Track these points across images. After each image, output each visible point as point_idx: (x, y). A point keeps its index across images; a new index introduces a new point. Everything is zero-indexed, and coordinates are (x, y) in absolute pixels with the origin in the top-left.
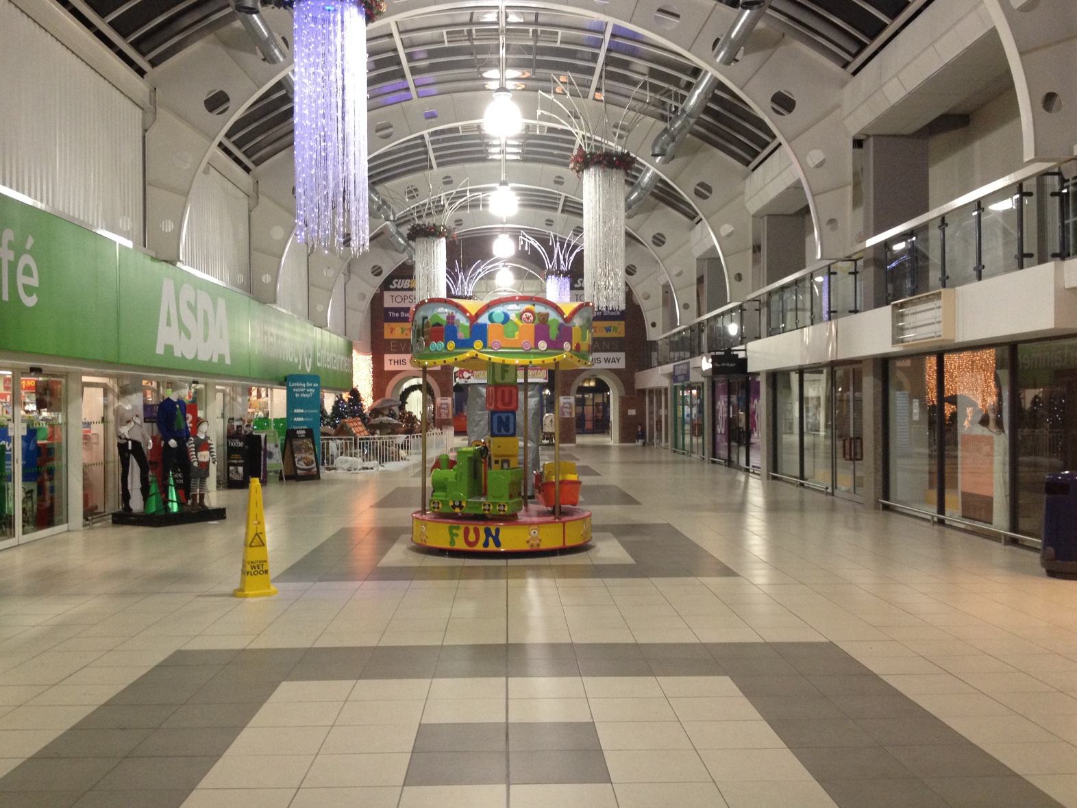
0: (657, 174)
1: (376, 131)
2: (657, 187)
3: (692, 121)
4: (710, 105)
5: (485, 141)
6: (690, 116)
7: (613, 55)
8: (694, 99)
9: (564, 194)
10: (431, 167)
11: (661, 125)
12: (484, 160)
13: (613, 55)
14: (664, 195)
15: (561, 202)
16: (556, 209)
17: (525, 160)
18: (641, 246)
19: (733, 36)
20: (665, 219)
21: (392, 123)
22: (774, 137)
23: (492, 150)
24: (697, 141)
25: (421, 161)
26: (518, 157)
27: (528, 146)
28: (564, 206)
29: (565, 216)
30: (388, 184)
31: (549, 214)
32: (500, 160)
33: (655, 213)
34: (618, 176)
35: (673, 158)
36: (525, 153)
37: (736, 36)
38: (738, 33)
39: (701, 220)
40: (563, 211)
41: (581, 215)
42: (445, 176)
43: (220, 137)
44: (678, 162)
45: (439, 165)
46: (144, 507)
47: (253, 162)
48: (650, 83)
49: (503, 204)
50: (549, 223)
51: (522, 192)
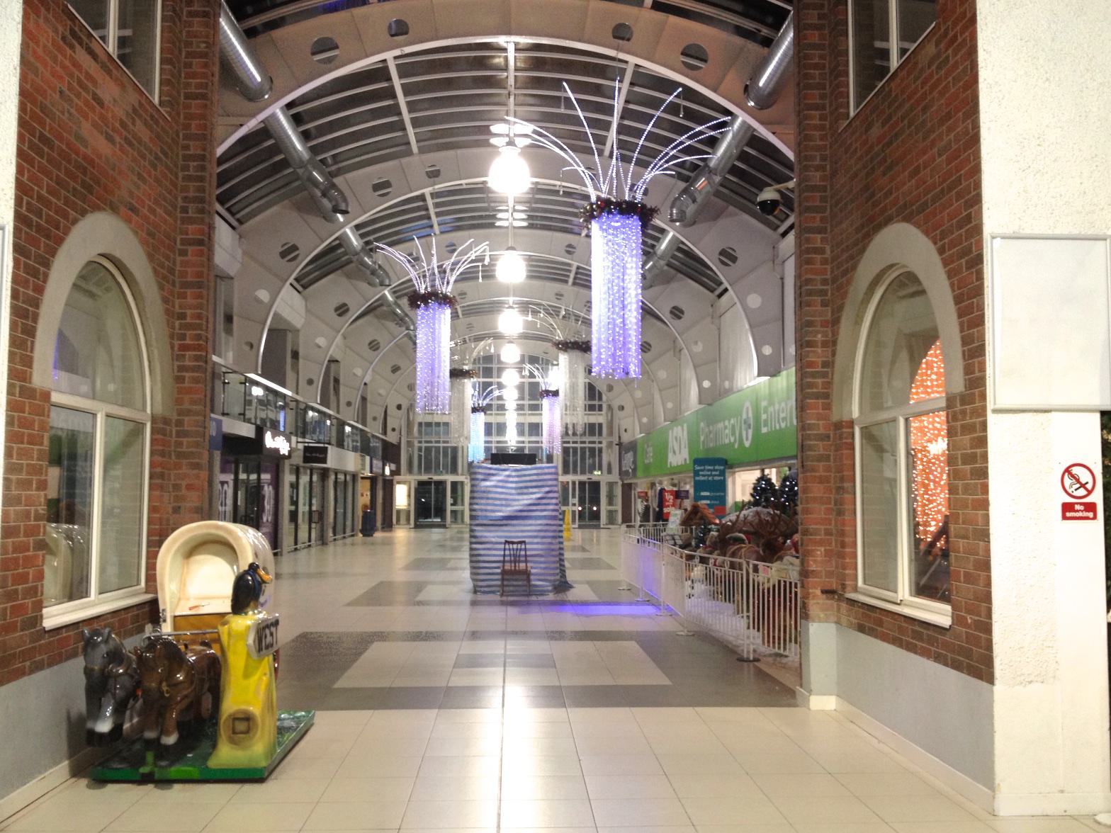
0: (750, 127)
1: (314, 54)
2: (674, 257)
3: (662, 262)
4: (747, 149)
5: (492, 205)
6: (661, 258)
7: (631, 106)
8: (664, 245)
9: (575, 264)
10: (410, 153)
11: (682, 185)
12: (492, 226)
13: (631, 106)
14: (687, 265)
15: (572, 275)
16: (566, 282)
17: (531, 226)
18: (659, 323)
19: (761, 84)
20: (686, 292)
21: (338, 41)
22: (721, 283)
23: (500, 215)
24: (673, 272)
25: (420, 218)
26: (525, 224)
27: (536, 203)
28: (575, 278)
29: (576, 289)
30: (349, 176)
31: (558, 287)
32: (507, 227)
33: (674, 285)
34: (577, 354)
35: (694, 223)
36: (530, 217)
37: (767, 82)
38: (770, 78)
39: (726, 290)
40: (574, 284)
41: (589, 287)
42: (447, 243)
43: (291, 280)
44: (656, 289)
45: (422, 151)
46: (51, 631)
47: (302, 286)
48: (685, 107)
49: (511, 268)
50: (559, 296)
51: (529, 259)
